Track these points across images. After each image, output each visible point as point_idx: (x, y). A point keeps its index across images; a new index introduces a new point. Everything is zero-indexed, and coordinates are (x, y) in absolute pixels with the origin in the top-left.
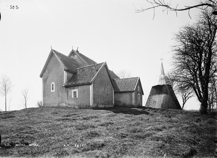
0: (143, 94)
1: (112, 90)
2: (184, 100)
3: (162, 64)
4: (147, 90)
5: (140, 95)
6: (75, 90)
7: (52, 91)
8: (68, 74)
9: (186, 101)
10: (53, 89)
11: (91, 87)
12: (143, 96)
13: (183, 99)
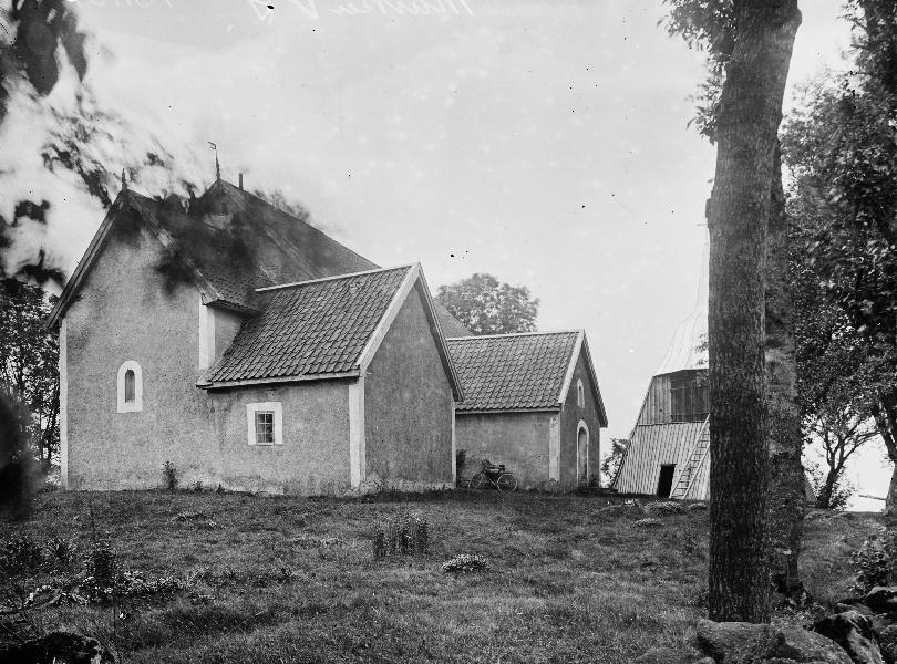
0: (604, 423)
1: (447, 403)
2: (833, 455)
3: (218, 165)
4: (624, 404)
5: (586, 429)
6: (266, 407)
7: (123, 407)
8: (219, 320)
9: (842, 459)
10: (130, 396)
11: (356, 393)
12: (602, 430)
13: (829, 449)
